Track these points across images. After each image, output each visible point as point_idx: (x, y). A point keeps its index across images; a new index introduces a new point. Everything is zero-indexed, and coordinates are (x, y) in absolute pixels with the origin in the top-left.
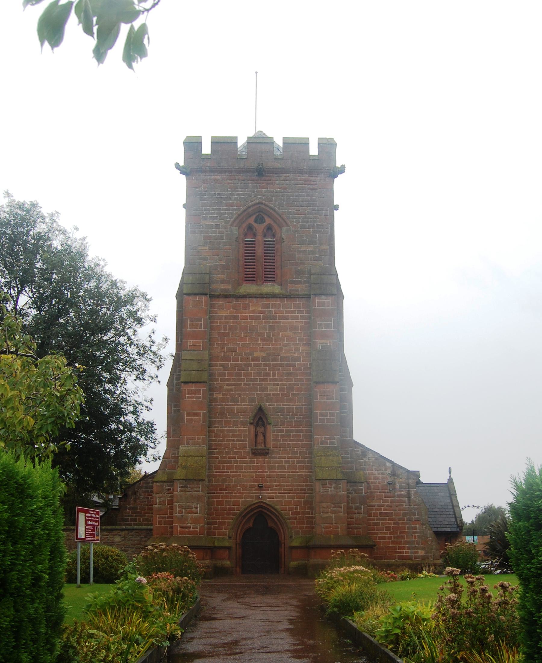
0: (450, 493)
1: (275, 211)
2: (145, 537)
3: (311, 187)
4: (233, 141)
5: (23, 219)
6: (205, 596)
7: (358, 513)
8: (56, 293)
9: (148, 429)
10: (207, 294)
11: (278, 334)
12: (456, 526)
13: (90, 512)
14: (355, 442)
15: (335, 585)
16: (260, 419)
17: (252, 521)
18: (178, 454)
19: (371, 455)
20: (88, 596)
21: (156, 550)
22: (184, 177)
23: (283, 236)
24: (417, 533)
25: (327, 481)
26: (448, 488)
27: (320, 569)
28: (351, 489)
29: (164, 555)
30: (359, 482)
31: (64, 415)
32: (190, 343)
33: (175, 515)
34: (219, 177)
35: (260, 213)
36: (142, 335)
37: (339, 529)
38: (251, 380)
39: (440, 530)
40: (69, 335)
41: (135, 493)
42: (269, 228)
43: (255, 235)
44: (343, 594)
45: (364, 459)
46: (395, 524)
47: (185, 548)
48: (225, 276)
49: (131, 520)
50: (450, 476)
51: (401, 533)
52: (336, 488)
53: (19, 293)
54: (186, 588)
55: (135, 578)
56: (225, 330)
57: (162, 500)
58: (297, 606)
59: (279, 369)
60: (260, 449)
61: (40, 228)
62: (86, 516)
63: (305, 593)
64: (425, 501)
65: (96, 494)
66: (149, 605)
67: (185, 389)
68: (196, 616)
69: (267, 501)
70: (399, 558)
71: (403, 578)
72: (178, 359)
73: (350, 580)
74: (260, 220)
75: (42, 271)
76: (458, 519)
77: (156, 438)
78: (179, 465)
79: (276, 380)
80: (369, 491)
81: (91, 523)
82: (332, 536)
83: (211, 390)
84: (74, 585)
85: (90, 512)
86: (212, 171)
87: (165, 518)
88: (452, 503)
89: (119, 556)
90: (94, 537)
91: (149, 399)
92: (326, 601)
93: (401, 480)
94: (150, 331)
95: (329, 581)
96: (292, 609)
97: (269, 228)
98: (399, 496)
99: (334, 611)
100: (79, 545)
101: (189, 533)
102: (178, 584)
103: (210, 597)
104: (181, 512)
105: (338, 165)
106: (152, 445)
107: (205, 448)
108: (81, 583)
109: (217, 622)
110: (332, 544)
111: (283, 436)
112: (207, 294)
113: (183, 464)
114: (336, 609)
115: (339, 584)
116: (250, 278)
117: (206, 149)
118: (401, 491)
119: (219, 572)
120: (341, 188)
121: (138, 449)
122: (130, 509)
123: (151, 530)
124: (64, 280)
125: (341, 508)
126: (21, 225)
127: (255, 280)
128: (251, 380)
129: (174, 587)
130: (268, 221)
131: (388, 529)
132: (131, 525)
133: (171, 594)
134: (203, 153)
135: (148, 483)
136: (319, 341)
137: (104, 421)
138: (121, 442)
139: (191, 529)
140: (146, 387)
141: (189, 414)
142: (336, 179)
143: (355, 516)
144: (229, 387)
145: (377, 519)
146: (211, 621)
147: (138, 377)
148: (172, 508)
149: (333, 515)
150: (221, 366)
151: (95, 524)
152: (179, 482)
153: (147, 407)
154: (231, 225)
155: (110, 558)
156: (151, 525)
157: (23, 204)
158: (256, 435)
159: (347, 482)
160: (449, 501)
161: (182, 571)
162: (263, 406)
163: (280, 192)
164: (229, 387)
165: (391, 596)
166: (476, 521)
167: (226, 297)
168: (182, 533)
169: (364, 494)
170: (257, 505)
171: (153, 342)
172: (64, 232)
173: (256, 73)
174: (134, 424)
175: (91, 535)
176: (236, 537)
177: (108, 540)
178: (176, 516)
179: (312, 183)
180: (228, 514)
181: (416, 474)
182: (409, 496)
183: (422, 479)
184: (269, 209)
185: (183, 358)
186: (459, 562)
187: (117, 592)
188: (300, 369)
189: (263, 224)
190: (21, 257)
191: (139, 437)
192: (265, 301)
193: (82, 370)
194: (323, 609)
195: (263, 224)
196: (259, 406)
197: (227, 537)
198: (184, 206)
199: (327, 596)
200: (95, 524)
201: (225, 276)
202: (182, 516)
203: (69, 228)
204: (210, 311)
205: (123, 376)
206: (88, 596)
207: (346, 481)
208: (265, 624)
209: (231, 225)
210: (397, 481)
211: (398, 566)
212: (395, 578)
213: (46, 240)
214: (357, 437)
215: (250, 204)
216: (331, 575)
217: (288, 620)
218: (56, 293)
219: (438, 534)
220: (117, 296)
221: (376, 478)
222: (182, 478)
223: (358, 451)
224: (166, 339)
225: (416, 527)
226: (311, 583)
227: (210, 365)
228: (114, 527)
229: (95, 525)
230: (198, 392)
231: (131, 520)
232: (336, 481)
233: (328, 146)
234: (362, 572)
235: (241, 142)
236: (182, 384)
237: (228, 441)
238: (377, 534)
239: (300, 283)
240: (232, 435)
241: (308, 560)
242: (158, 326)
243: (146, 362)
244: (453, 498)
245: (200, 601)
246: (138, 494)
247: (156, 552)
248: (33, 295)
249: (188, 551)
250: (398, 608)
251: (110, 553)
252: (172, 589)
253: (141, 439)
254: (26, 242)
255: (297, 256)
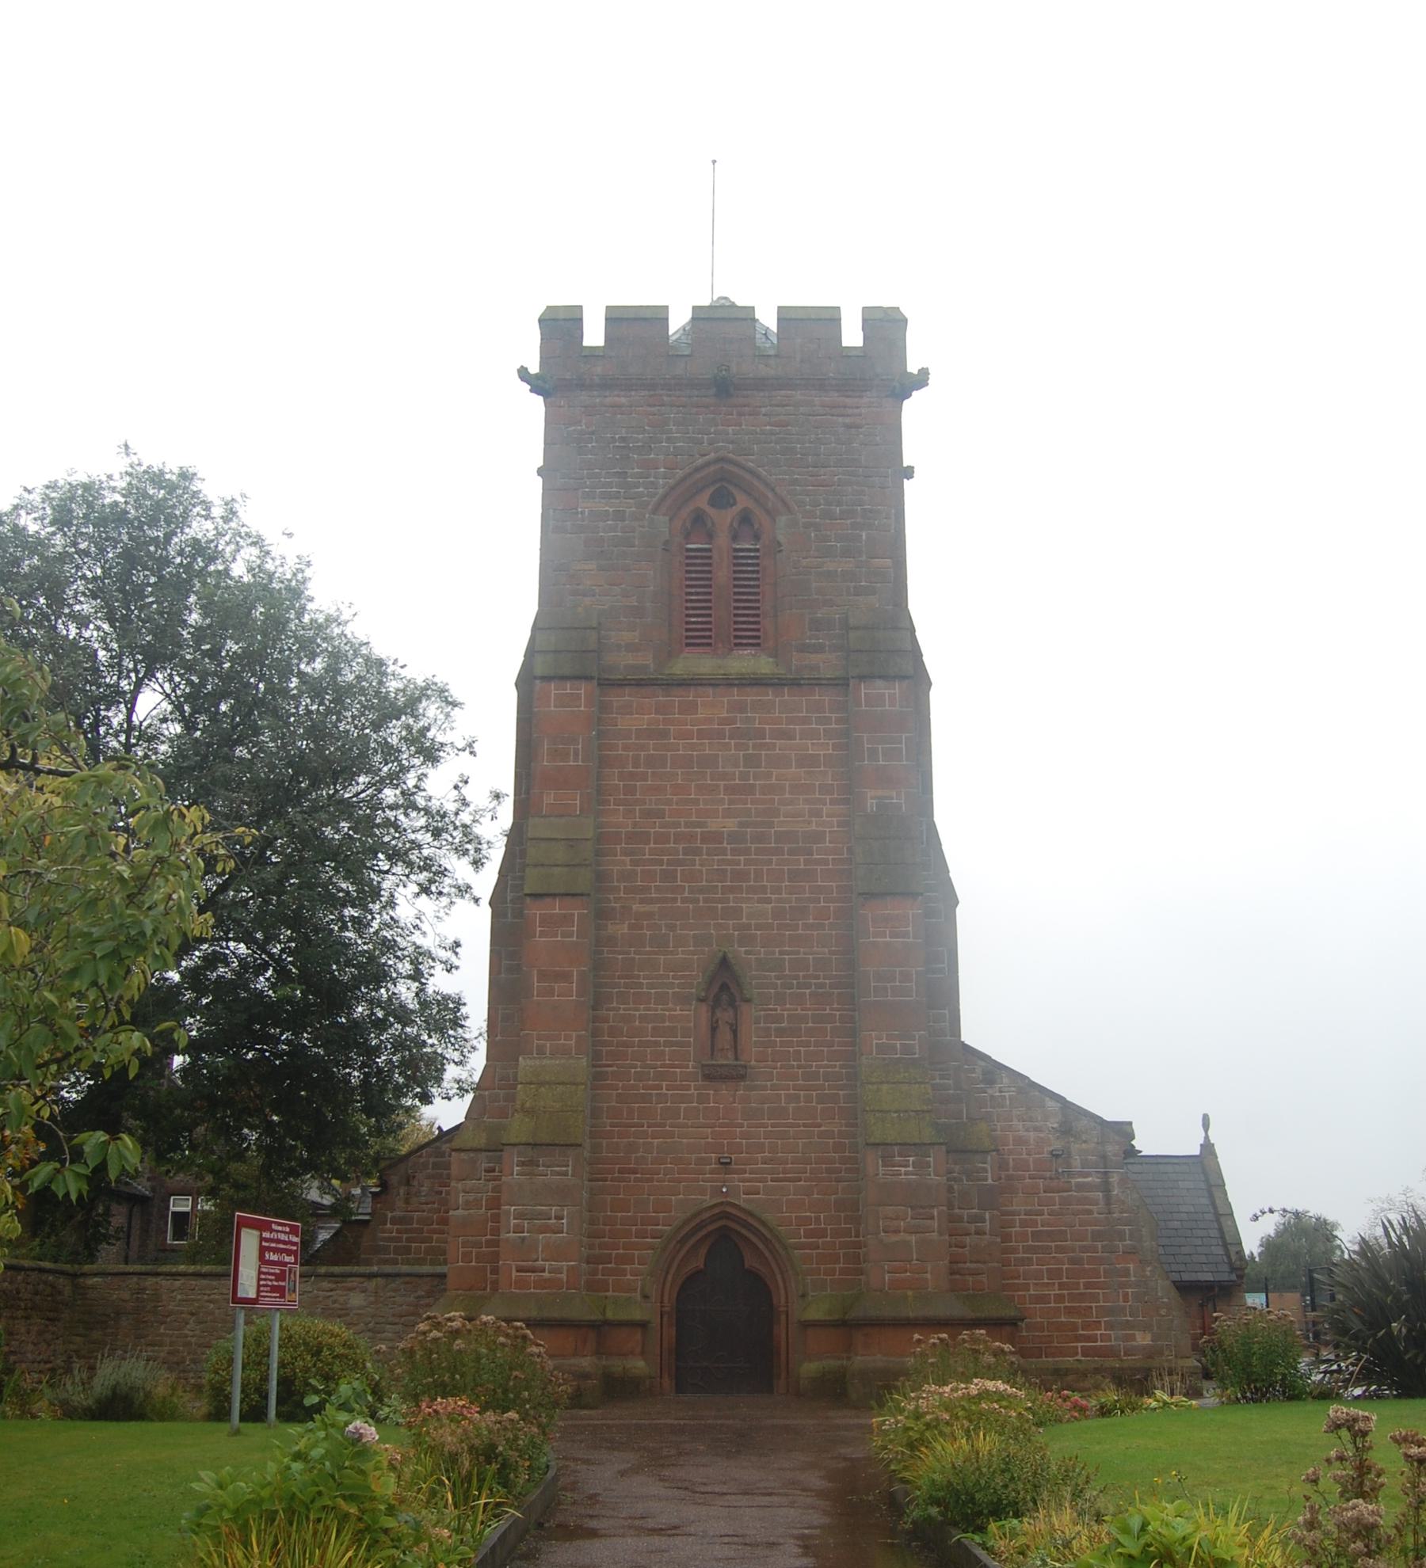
0: (1207, 1181)
1: (758, 477)
2: (429, 1294)
3: (848, 420)
4: (656, 317)
5: (159, 506)
6: (575, 1460)
7: (977, 1233)
8: (231, 686)
9: (445, 1015)
10: (592, 678)
11: (769, 776)
12: (1226, 1268)
13: (274, 1226)
14: (966, 1048)
15: (928, 1434)
16: (724, 987)
17: (703, 1251)
18: (515, 1079)
19: (1005, 1080)
20: (200, 1480)
21: (435, 1334)
22: (539, 400)
23: (781, 538)
24: (1130, 1287)
25: (896, 1148)
26: (1203, 1168)
27: (882, 1387)
28: (957, 1168)
29: (455, 1347)
30: (977, 1152)
31: (142, 934)
32: (549, 798)
33: (504, 1236)
34: (623, 400)
35: (722, 482)
36: (437, 785)
37: (929, 1276)
38: (701, 891)
39: (1186, 1277)
40: (257, 786)
41: (408, 1181)
42: (746, 518)
43: (710, 536)
44: (954, 1467)
45: (990, 1091)
46: (1072, 1261)
47: (517, 1328)
48: (636, 634)
49: (397, 1250)
50: (1207, 1137)
51: (1087, 1286)
52: (920, 1166)
53: (139, 686)
54: (512, 1443)
55: (347, 1424)
56: (636, 765)
57: (471, 1197)
58: (821, 1494)
59: (770, 862)
60: (722, 1066)
61: (199, 528)
62: (262, 1239)
63: (842, 1451)
64: (1148, 1201)
65: (316, 1183)
66: (382, 1507)
67: (536, 911)
68: (540, 1525)
69: (742, 1200)
70: (1086, 1352)
71: (1104, 1411)
72: (516, 838)
73: (971, 1421)
74: (721, 499)
75: (200, 634)
76: (1233, 1250)
77: (467, 1036)
78: (518, 1107)
79: (764, 889)
80: (1003, 1174)
81: (274, 1257)
82: (910, 1293)
83: (602, 915)
84: (225, 1427)
85: (274, 1226)
86: (607, 384)
87: (479, 1245)
88: (1215, 1207)
89: (350, 1347)
90: (282, 1296)
91: (450, 941)
92: (903, 1481)
93: (1084, 1146)
94: (456, 779)
95: (910, 1424)
96: (809, 1500)
97: (746, 518)
98: (1081, 1187)
99: (929, 1516)
100: (241, 1318)
101: (542, 1284)
102: (490, 1432)
103: (587, 1462)
104: (519, 1229)
105: (913, 367)
106: (456, 1056)
107: (584, 1062)
108: (243, 1419)
109: (597, 1543)
110: (911, 1315)
111: (781, 1032)
112: (592, 678)
113: (528, 1105)
114: (934, 1511)
115: (941, 1433)
116: (699, 638)
117: (594, 335)
118: (1087, 1175)
119: (618, 1389)
120: (920, 424)
121: (423, 1073)
122: (394, 1221)
123: (443, 1276)
124: (250, 659)
125: (932, 1218)
126: (153, 523)
127: (709, 645)
128: (701, 891)
129: (477, 1442)
130: (742, 501)
131: (1054, 1274)
132: (395, 1262)
133: (466, 1462)
134: (585, 344)
135: (442, 1155)
136: (870, 793)
137: (336, 998)
138: (377, 1051)
139: (546, 1275)
140: (441, 914)
141: (543, 976)
142: (906, 403)
143: (968, 1239)
144: (647, 908)
145: (1028, 1249)
146: (580, 1543)
147: (425, 890)
148: (496, 1218)
149: (913, 1238)
150: (626, 855)
151: (287, 1259)
152: (516, 1150)
153: (445, 963)
154: (655, 511)
155: (326, 1352)
156: (445, 1262)
157: (162, 473)
158: (714, 1029)
159: (948, 1152)
160: (1205, 1201)
161: (505, 1391)
162: (730, 956)
163: (772, 433)
164: (647, 908)
165: (1091, 1470)
166: (1260, 1254)
167: (639, 683)
168: (521, 1284)
169: (990, 1181)
170: (716, 1211)
171: (465, 803)
172: (258, 542)
173: (714, 162)
174: (413, 1005)
175: (274, 1289)
176: (662, 1296)
177: (335, 1302)
178: (507, 1240)
179: (850, 411)
180: (641, 1234)
181: (1123, 1131)
182: (1106, 1188)
183: (1137, 1143)
184: (742, 473)
185: (530, 835)
186: (1250, 1365)
187: (289, 1468)
188: (825, 862)
189: (732, 513)
190: (151, 599)
191: (425, 1037)
192: (735, 695)
193: (248, 840)
194: (895, 1505)
195: (732, 513)
196: (721, 954)
197: (639, 1297)
198: (540, 472)
199: (906, 1468)
200: (287, 1259)
201: (636, 634)
202: (524, 1239)
203: (272, 537)
204: (599, 719)
205: (385, 885)
206: (200, 1480)
207: (944, 1148)
208: (732, 1554)
209: (655, 511)
210: (1075, 1147)
211: (1084, 1375)
212: (1083, 1410)
213: (212, 559)
214: (971, 1035)
215: (700, 461)
216: (917, 1407)
217: (797, 1538)
218: (231, 686)
219: (1185, 1289)
220: (377, 693)
221: (1020, 1141)
222: (524, 1140)
223: (973, 1071)
224: (497, 796)
225: (1128, 1269)
226: (856, 1421)
227: (598, 853)
228: (348, 1269)
229: (285, 1264)
230: (567, 919)
231: (397, 1250)
232: (921, 1148)
233: (885, 326)
234: (1000, 1396)
235: (678, 320)
236: (528, 900)
237: (641, 1044)
238: (1026, 1287)
239: (819, 649)
240: (653, 1028)
241: (848, 1358)
242: (475, 768)
243: (444, 851)
244: (1217, 1194)
245: (555, 1478)
246: (415, 1183)
247: (435, 1340)
248: (174, 691)
249: (525, 1337)
250: (1135, 1523)
251: (326, 1339)
252: (471, 1448)
253: (430, 1041)
254: (166, 561)
255: (814, 585)
